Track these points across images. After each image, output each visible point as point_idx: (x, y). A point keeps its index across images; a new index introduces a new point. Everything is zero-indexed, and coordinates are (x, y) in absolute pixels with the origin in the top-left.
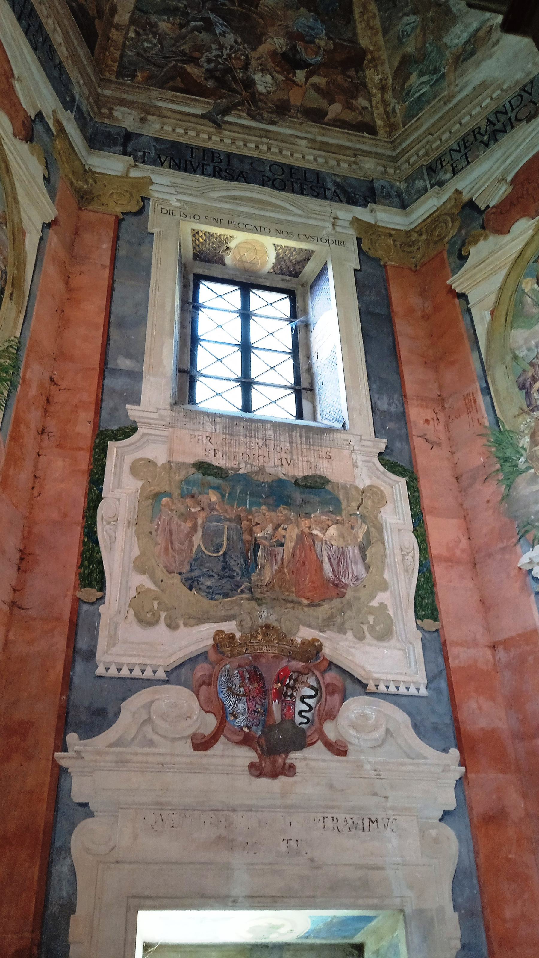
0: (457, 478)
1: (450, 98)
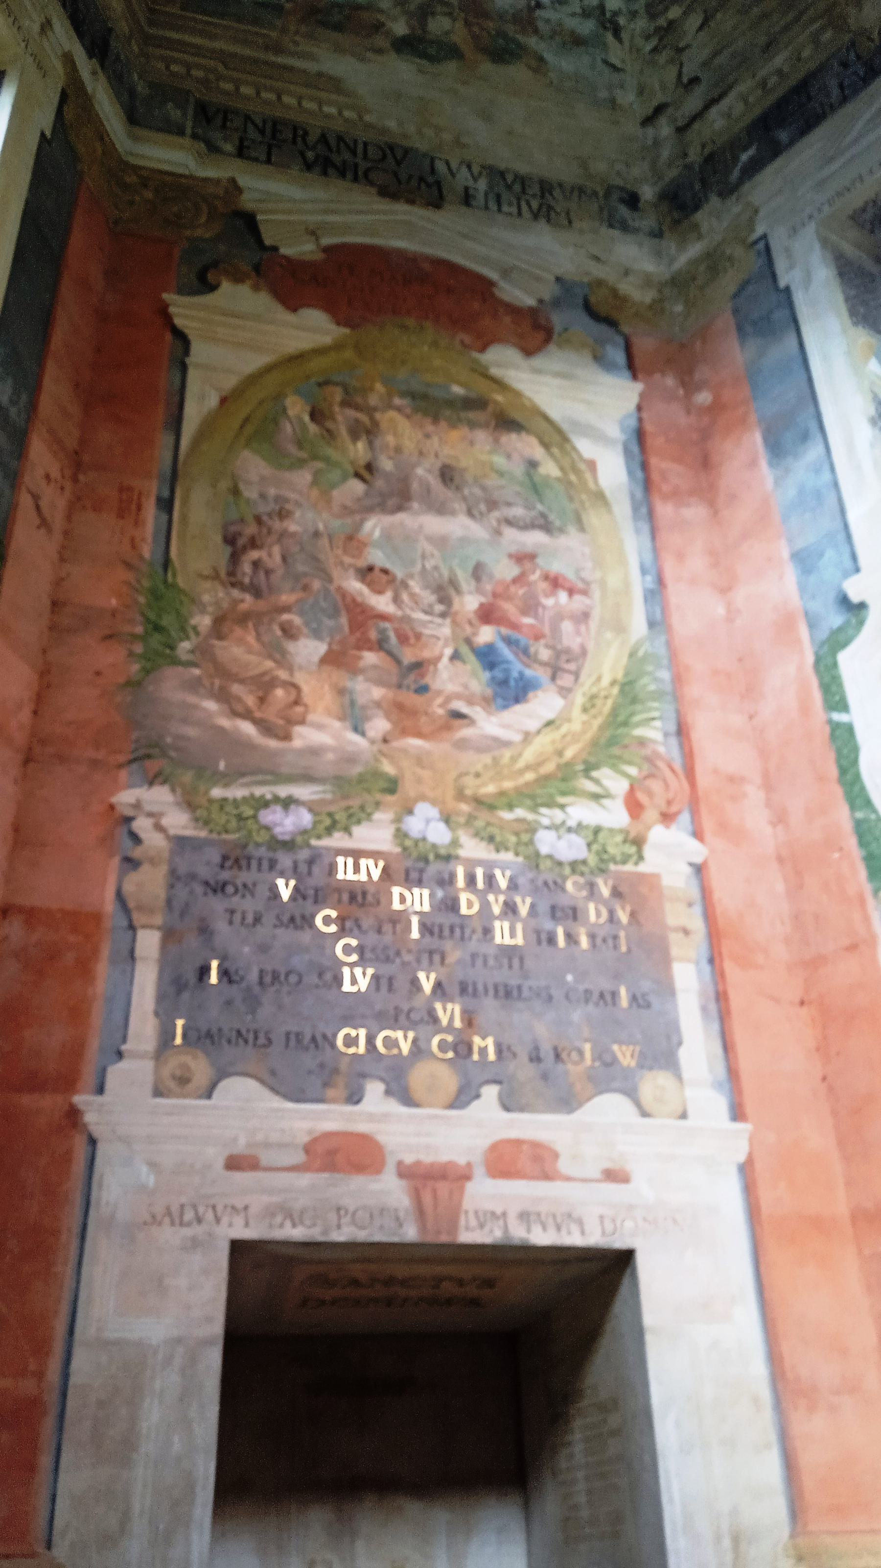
0: (54, 604)
1: (278, 49)
